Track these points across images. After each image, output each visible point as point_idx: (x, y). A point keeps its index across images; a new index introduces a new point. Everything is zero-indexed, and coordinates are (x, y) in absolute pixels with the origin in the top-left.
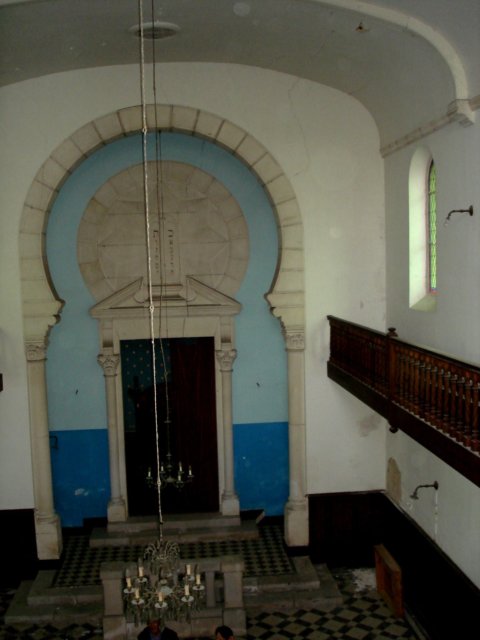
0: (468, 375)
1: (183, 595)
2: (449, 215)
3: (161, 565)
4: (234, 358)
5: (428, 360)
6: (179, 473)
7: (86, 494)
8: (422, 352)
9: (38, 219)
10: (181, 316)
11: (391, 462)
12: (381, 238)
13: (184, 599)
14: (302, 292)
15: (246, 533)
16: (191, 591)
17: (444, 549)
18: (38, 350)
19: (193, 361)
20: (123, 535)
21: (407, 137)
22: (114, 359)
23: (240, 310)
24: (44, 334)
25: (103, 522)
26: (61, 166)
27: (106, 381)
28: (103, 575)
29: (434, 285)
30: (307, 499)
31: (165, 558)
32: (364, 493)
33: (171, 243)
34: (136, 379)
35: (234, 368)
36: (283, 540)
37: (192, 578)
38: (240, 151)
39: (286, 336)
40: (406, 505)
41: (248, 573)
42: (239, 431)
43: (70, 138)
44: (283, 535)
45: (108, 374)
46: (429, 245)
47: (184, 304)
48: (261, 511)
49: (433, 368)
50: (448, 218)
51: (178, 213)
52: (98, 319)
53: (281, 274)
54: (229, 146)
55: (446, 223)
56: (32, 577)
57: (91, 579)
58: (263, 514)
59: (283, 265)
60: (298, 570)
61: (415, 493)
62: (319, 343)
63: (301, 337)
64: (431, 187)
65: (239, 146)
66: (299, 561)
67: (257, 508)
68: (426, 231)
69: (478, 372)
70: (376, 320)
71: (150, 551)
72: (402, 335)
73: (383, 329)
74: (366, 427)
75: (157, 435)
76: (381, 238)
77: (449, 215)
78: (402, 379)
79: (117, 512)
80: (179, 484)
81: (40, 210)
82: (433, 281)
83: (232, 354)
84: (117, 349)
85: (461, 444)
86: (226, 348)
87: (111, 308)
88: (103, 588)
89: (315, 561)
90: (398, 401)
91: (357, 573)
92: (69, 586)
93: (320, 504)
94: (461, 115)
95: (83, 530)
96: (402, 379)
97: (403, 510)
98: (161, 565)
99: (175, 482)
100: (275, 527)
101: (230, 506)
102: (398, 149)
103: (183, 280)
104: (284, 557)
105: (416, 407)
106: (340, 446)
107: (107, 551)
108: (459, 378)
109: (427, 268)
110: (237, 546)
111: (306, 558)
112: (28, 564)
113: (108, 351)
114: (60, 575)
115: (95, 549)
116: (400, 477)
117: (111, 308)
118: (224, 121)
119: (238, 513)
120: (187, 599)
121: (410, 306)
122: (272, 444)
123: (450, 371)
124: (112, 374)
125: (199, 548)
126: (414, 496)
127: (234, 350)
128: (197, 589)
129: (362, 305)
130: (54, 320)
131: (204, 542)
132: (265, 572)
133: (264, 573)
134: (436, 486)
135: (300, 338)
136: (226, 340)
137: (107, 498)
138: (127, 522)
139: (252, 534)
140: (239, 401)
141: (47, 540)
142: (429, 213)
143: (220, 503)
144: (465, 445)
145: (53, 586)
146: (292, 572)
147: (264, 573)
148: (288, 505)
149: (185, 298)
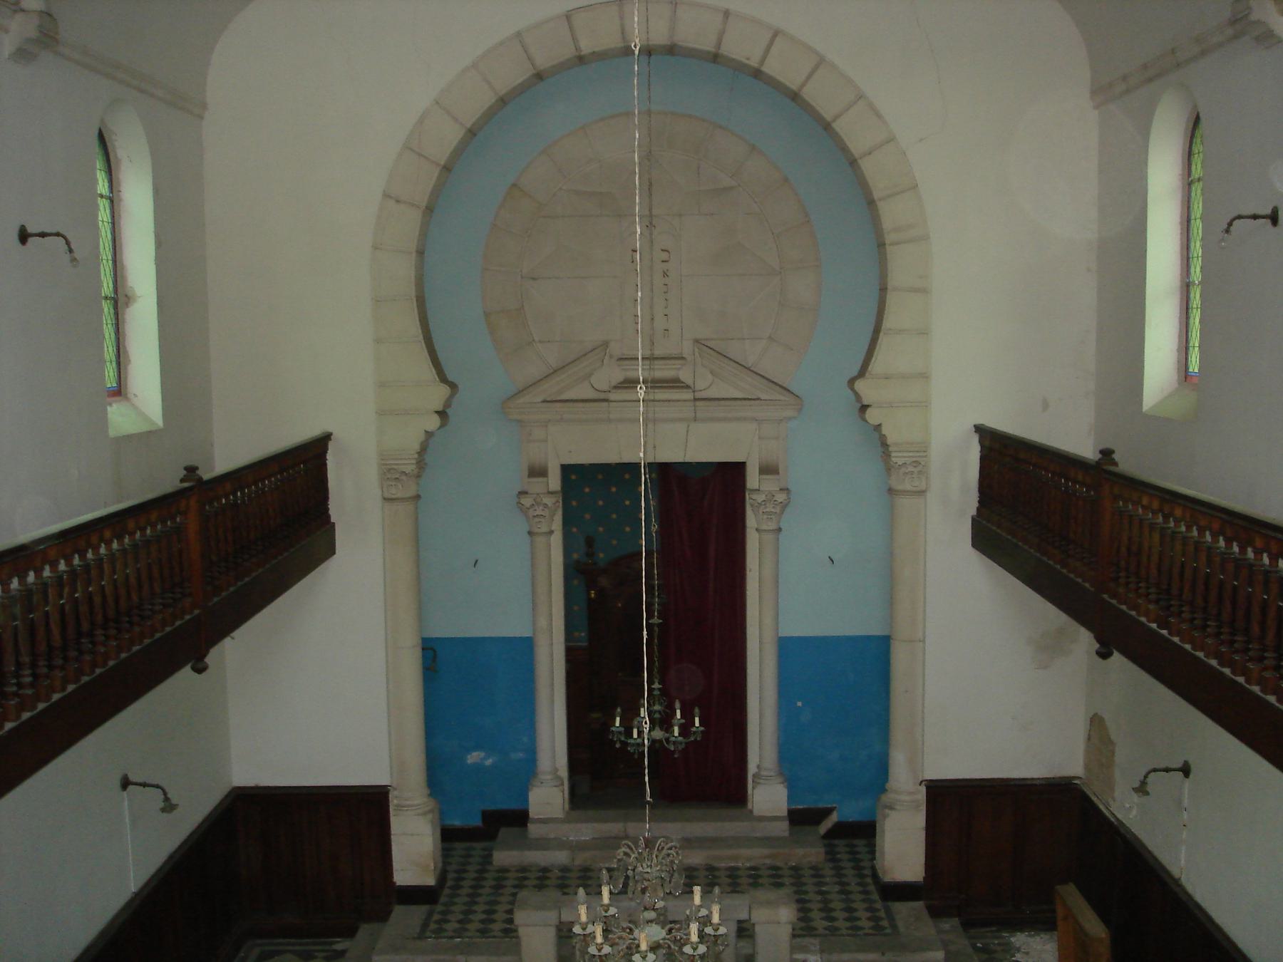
0: (1259, 542)
1: (687, 941)
2: (1230, 224)
3: (646, 883)
4: (784, 506)
5: (1178, 512)
6: (675, 721)
7: (489, 762)
8: (1167, 497)
9: (410, 220)
10: (681, 420)
11: (1096, 722)
12: (1089, 270)
13: (687, 949)
14: (924, 376)
15: (800, 851)
16: (702, 935)
17: (1198, 897)
18: (404, 478)
19: (706, 507)
20: (561, 844)
21: (1145, 66)
22: (549, 501)
23: (800, 410)
24: (417, 447)
25: (519, 818)
26: (456, 120)
27: (532, 543)
28: (520, 917)
29: (1194, 366)
30: (923, 789)
31: (655, 869)
32: (1037, 782)
33: (665, 274)
34: (590, 542)
35: (782, 525)
36: (873, 868)
37: (704, 912)
38: (808, 93)
39: (891, 466)
40: (1125, 808)
41: (801, 929)
42: (788, 648)
43: (475, 65)
44: (873, 852)
45: (537, 530)
46: (1186, 287)
47: (687, 395)
48: (828, 812)
49: (1189, 528)
50: (1227, 231)
51: (680, 215)
52: (519, 421)
53: (883, 340)
54: (788, 84)
55: (1223, 240)
56: (382, 916)
57: (497, 927)
58: (834, 818)
59: (888, 323)
60: (902, 929)
61: (1143, 783)
62: (956, 479)
63: (919, 465)
64: (1193, 167)
65: (803, 85)
66: (905, 910)
67: (821, 805)
68: (1182, 255)
69: (1280, 536)
70: (1076, 437)
71: (626, 854)
72: (1127, 464)
73: (1087, 450)
74: (1049, 648)
75: (645, 633)
76: (1089, 270)
77: (1230, 224)
78: (1123, 549)
79: (547, 798)
80: (674, 743)
81: (413, 205)
82: (1194, 359)
83: (781, 497)
84: (555, 481)
85: (1241, 680)
86: (770, 484)
87: (544, 401)
88: (518, 944)
89: (936, 913)
90: (1114, 596)
91: (1019, 939)
92: (452, 938)
93: (949, 801)
94: (1258, 22)
95: (485, 829)
96: (1123, 549)
97: (1117, 819)
98: (646, 883)
99: (667, 740)
100: (856, 842)
101: (769, 797)
102: (1128, 91)
103: (687, 348)
104: (875, 902)
105: (1151, 607)
106: (992, 686)
107: (527, 874)
108: (1243, 550)
109: (1180, 318)
110: (781, 876)
111: (919, 904)
112: (375, 895)
113: (537, 485)
114: (436, 917)
115: (504, 870)
116: (1113, 752)
117: (544, 401)
118: (776, 34)
119: (785, 813)
120: (695, 949)
121: (1145, 408)
122: (856, 679)
123: (1223, 534)
124: (545, 529)
125: (707, 877)
126: (1142, 789)
127: (785, 490)
128: (712, 933)
129: (1046, 406)
130: (433, 423)
131: (716, 865)
132: (837, 929)
133: (833, 931)
134: (1186, 770)
135: (920, 468)
136: (768, 470)
137: (528, 771)
138: (566, 820)
139: (810, 853)
140: (791, 591)
141: (413, 850)
142: (1189, 221)
143: (750, 791)
144: (1248, 681)
145: (421, 936)
146: (888, 931)
147: (833, 931)
148: (885, 798)
149: (689, 381)
